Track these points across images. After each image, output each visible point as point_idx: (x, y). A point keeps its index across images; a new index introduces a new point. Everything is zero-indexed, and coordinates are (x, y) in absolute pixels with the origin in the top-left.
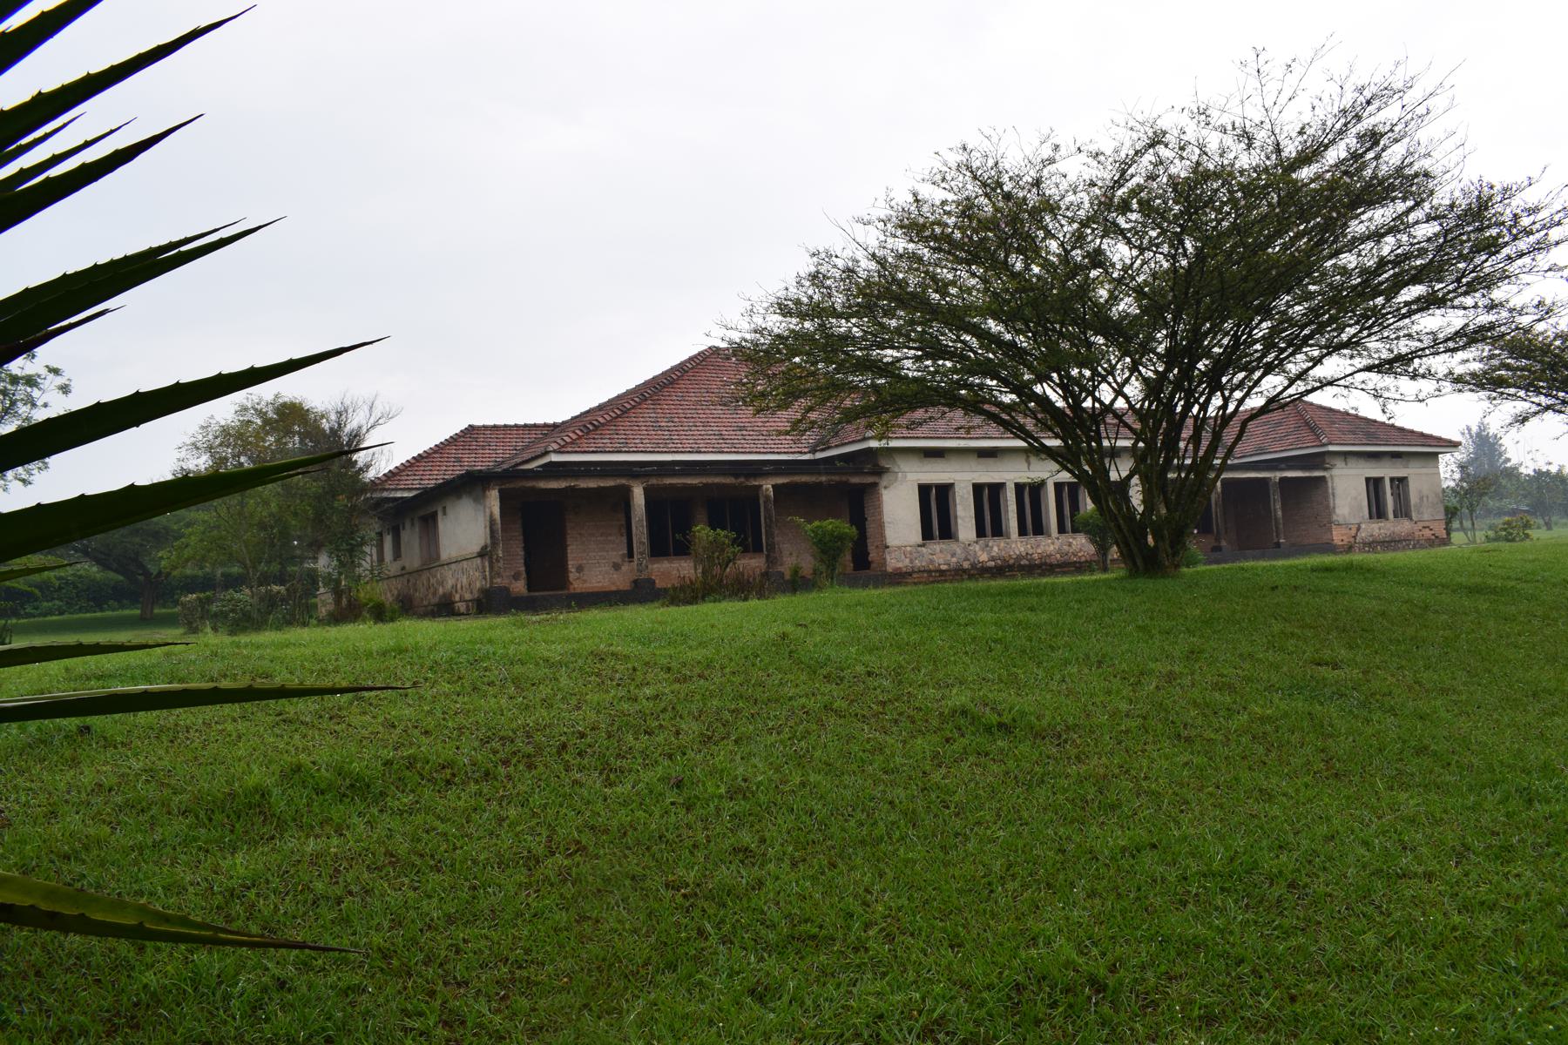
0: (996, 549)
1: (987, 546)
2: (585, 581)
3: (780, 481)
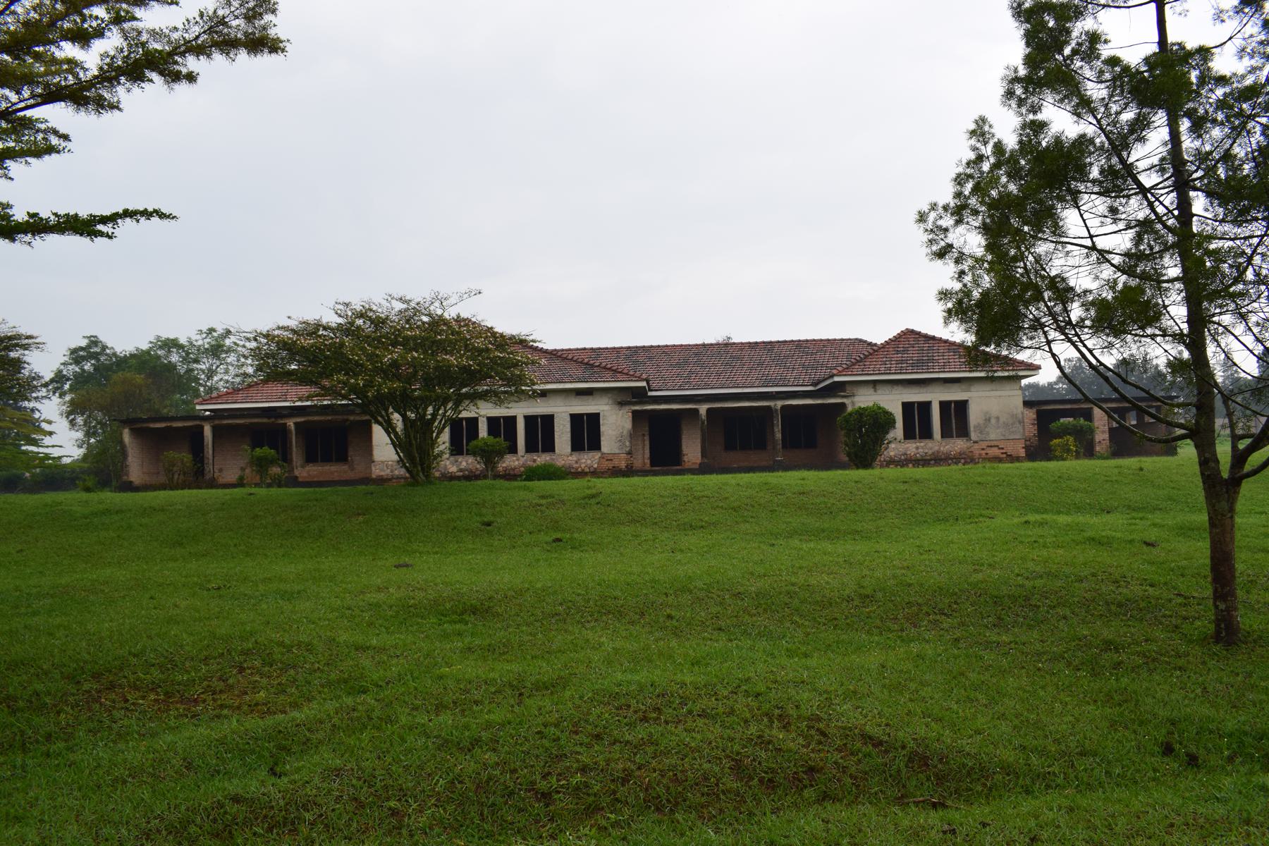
0: (464, 464)
1: (457, 461)
2: (223, 478)
3: (299, 420)
